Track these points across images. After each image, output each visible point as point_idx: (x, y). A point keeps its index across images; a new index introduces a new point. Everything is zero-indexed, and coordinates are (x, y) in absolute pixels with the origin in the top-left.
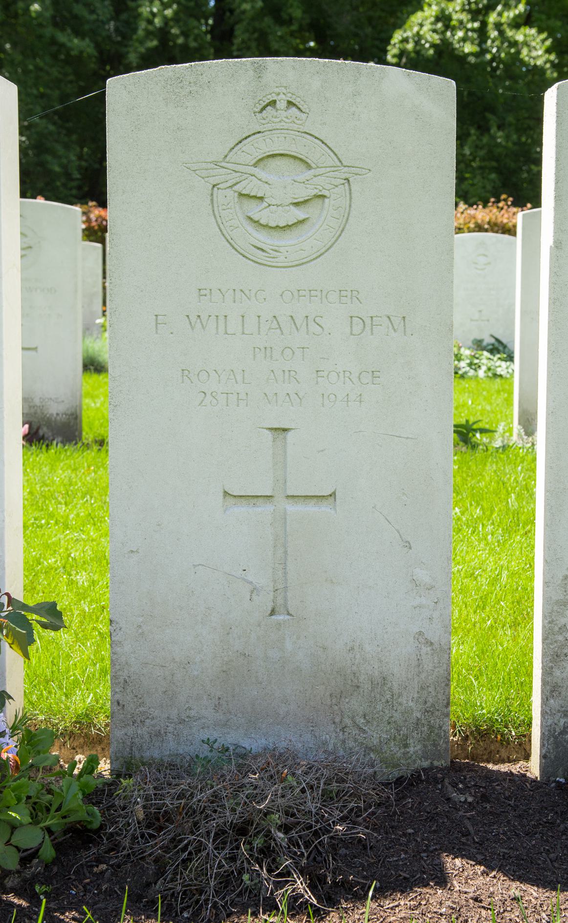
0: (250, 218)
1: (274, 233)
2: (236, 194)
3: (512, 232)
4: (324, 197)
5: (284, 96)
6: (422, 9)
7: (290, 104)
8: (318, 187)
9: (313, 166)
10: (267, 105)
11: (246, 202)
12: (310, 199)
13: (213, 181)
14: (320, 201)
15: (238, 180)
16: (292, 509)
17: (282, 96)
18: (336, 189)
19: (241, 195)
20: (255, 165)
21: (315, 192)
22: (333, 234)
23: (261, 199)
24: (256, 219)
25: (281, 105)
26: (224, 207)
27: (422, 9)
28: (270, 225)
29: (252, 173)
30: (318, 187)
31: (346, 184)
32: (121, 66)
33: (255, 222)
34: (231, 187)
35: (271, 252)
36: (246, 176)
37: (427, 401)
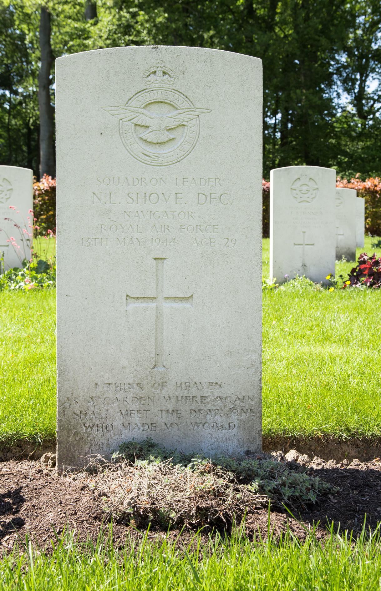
0: (141, 138)
1: (157, 146)
2: (133, 125)
3: (34, 151)
4: (184, 125)
5: (161, 69)
6: (247, 485)
7: (165, 73)
8: (181, 120)
9: (178, 108)
10: (150, 74)
11: (138, 127)
12: (176, 127)
13: (121, 116)
14: (183, 126)
15: (134, 116)
16: (167, 306)
17: (159, 69)
18: (192, 121)
19: (136, 125)
20: (144, 108)
21: (178, 123)
22: (190, 147)
23: (148, 127)
24: (145, 139)
25: (159, 73)
26: (126, 132)
27: (247, 485)
28: (148, 140)
29: (143, 113)
30: (181, 120)
31: (198, 118)
32: (273, 167)
33: (144, 140)
34: (130, 120)
35: (153, 157)
36: (138, 114)
37: (251, 537)
